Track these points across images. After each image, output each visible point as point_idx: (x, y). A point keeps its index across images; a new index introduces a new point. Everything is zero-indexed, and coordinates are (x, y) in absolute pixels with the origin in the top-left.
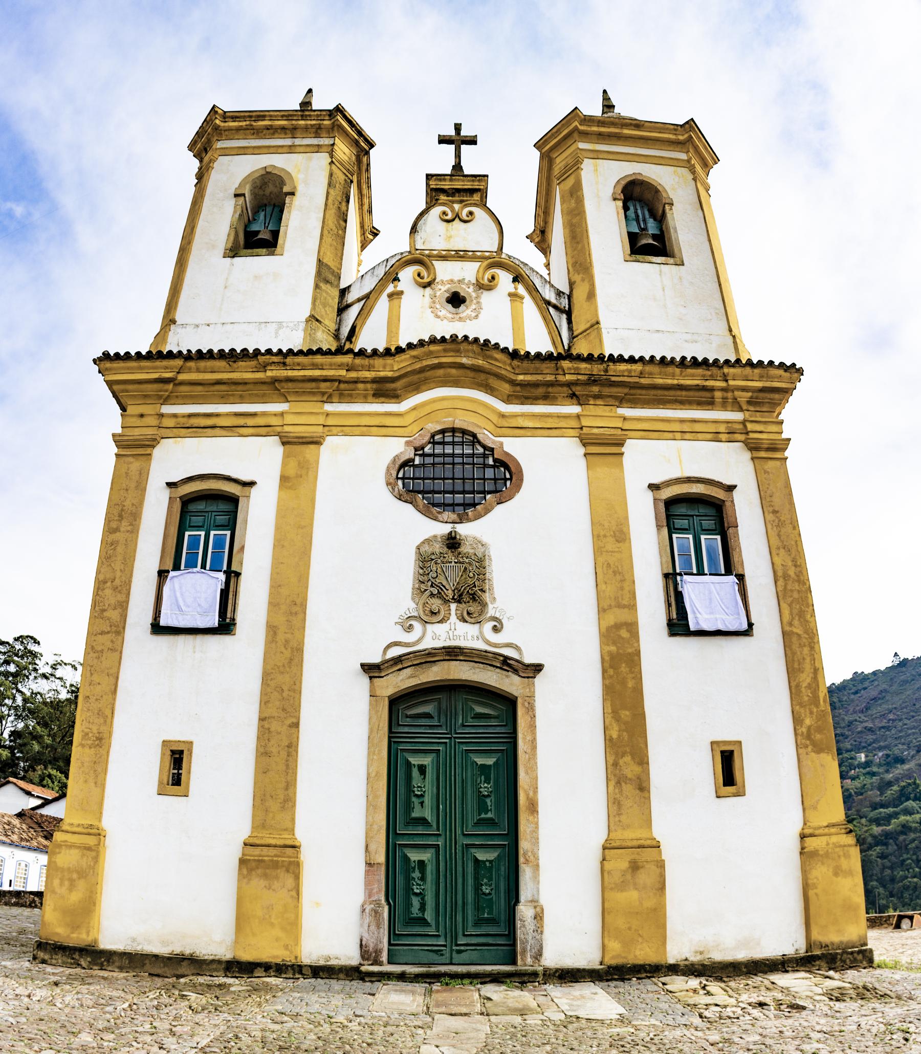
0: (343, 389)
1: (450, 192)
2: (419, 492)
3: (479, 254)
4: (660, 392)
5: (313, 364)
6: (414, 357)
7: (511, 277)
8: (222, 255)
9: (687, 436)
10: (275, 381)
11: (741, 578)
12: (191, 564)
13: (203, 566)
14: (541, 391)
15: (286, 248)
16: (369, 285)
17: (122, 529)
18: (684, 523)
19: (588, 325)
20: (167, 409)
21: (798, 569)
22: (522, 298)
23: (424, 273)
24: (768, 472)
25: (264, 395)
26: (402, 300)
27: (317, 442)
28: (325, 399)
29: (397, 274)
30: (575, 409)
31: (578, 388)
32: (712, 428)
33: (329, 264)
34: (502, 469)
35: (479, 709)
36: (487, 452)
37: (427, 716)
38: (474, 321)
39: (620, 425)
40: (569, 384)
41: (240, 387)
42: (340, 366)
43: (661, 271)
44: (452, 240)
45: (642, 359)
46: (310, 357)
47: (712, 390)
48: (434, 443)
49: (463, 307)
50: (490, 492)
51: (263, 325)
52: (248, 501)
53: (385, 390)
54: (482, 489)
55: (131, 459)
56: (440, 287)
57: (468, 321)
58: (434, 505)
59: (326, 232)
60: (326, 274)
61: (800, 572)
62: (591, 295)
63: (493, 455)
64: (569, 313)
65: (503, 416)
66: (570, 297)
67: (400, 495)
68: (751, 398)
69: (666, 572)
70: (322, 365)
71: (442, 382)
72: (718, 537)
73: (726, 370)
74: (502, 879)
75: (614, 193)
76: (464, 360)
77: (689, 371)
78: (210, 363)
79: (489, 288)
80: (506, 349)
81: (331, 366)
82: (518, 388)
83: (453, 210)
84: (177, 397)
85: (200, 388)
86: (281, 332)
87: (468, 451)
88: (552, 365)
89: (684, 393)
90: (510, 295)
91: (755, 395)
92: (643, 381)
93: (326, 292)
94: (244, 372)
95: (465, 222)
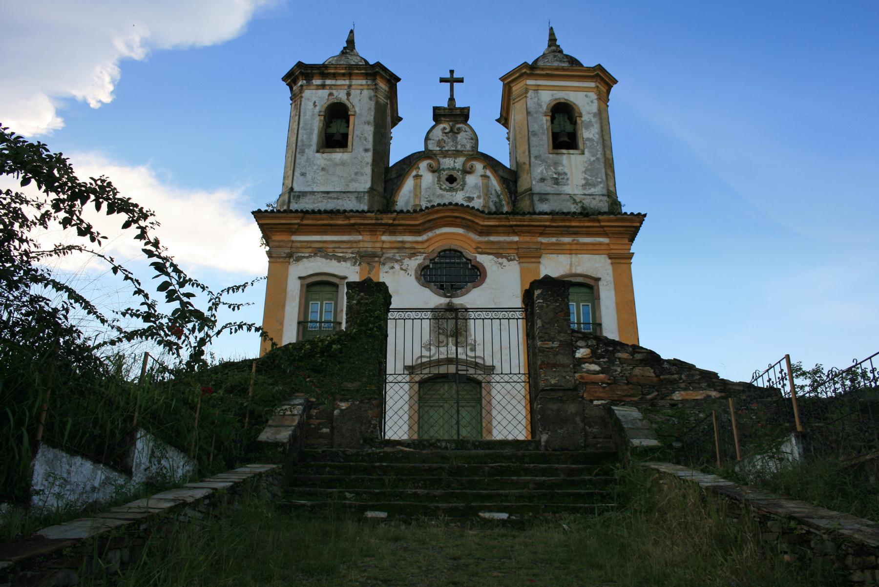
10: (354, 225)
74: (305, 222)
79: (470, 173)
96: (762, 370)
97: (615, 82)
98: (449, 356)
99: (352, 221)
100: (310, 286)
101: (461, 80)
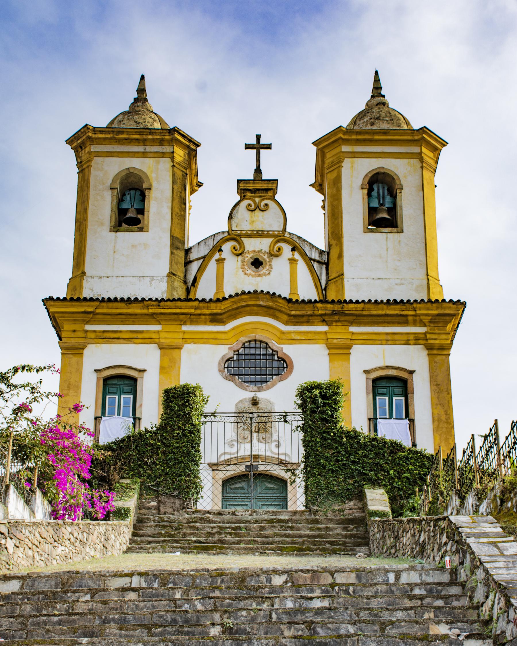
0: (193, 319)
1: (253, 190)
2: (237, 375)
3: (271, 233)
4: (374, 318)
5: (176, 306)
6: (233, 302)
7: (290, 248)
8: (109, 230)
9: (390, 342)
10: (153, 314)
11: (412, 421)
12: (111, 414)
13: (119, 414)
14: (305, 319)
15: (150, 227)
16: (204, 251)
17: (70, 394)
18: (384, 390)
19: (337, 275)
20: (88, 327)
21: (448, 416)
22: (297, 261)
23: (238, 247)
24: (437, 363)
25: (147, 321)
26: (225, 264)
27: (179, 348)
28: (182, 323)
29: (221, 247)
30: (324, 328)
31: (326, 317)
32: (405, 337)
33: (178, 236)
34: (282, 362)
35: (270, 486)
36: (274, 353)
37: (242, 488)
38: (268, 276)
39: (350, 337)
40: (321, 315)
41: (133, 317)
42: (191, 307)
43: (387, 238)
44: (254, 224)
45: (363, 301)
46: (174, 302)
47: (406, 316)
48: (244, 348)
49: (261, 268)
50: (275, 375)
51: (142, 278)
52: (143, 380)
53: (216, 319)
54: (271, 373)
55: (71, 356)
56: (247, 255)
57: (264, 276)
58: (245, 382)
59: (174, 216)
60: (177, 242)
61: (449, 418)
62: (340, 256)
63: (277, 354)
64: (327, 264)
65: (283, 333)
66: (328, 253)
67: (226, 377)
68: (431, 319)
69: (369, 417)
70: (181, 306)
71: (249, 313)
72: (403, 398)
73: (415, 305)
75: (362, 185)
76: (261, 303)
77: (392, 306)
78: (115, 304)
79: (277, 256)
80: (285, 298)
81: (186, 307)
82: (292, 318)
83: (255, 202)
84: (95, 321)
85: (109, 317)
86: (153, 283)
87: (263, 352)
88: (311, 305)
89: (389, 318)
90: (289, 259)
91: (434, 318)
92: (364, 313)
93: (178, 255)
94: (135, 309)
95: (263, 211)
96: (449, 452)
97: (444, 144)
98: (253, 453)
99: (151, 311)
100: (106, 380)
101: (269, 147)
